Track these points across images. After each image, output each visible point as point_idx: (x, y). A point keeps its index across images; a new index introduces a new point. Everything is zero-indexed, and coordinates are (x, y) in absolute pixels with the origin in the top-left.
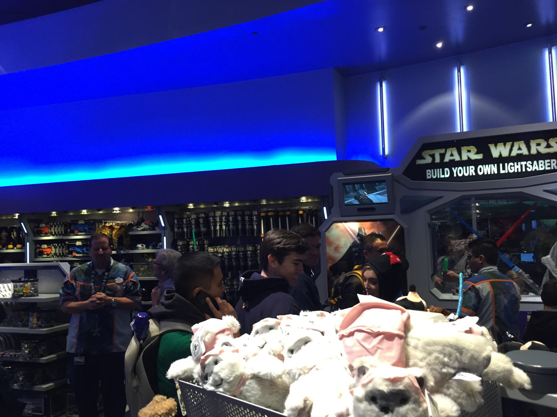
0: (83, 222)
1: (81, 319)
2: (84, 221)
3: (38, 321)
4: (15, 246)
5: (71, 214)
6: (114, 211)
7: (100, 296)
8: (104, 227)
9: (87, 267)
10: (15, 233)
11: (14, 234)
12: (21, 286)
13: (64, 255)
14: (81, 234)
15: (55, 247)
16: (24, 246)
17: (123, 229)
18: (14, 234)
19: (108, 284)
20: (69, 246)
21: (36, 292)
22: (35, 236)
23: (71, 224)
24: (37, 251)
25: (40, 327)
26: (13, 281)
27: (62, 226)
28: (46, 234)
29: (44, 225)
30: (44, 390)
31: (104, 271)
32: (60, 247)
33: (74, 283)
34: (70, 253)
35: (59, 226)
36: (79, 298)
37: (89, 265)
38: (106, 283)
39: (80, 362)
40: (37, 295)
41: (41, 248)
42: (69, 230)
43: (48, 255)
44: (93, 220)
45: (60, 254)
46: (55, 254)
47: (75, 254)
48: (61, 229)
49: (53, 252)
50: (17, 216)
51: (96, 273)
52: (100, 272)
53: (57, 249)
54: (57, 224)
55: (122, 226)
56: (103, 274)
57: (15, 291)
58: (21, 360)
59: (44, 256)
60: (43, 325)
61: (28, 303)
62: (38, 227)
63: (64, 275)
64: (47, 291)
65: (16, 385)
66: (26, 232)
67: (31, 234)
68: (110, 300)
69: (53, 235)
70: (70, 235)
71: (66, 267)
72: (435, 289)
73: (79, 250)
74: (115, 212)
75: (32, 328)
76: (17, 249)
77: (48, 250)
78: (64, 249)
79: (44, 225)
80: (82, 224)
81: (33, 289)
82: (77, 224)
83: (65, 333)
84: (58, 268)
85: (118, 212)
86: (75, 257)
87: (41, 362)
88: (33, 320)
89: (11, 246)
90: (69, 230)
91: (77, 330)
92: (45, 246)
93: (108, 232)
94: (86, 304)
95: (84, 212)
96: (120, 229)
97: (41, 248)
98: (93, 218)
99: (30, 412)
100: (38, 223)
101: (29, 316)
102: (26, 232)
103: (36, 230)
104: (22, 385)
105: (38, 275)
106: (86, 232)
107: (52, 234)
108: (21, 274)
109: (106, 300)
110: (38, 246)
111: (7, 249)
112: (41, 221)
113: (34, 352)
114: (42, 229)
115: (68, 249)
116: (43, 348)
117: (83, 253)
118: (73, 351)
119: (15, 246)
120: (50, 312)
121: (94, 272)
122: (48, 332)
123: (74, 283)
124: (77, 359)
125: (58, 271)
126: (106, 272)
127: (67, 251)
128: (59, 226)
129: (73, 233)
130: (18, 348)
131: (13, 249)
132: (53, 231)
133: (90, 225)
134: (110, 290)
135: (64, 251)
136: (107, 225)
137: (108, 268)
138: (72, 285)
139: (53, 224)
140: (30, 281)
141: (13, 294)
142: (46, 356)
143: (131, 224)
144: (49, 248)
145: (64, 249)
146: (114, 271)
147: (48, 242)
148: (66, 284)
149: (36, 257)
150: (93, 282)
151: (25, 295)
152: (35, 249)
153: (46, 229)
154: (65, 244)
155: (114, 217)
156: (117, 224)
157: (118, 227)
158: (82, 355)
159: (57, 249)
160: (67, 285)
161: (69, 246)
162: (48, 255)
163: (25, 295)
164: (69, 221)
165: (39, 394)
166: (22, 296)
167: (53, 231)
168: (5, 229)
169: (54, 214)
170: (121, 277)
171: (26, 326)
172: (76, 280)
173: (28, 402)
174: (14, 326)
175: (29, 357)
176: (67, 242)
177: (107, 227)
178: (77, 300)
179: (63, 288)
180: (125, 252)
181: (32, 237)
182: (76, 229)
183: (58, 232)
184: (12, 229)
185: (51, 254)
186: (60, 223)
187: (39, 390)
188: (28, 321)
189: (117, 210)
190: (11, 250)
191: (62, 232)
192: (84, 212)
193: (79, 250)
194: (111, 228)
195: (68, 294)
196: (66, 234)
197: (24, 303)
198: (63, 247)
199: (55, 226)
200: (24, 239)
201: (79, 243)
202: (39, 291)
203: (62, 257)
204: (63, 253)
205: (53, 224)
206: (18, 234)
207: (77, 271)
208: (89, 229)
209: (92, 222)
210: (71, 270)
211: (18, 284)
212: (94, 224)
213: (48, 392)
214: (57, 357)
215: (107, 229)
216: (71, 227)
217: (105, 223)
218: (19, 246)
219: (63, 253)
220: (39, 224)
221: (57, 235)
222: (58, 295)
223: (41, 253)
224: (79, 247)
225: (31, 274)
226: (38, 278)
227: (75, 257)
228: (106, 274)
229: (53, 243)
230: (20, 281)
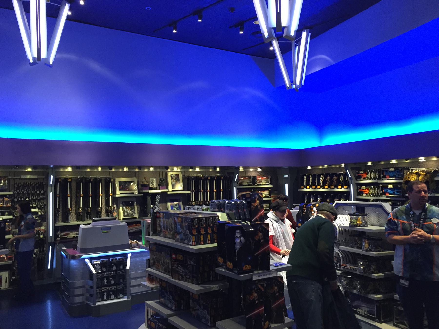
0: (393, 169)
1: (405, 250)
2: (394, 168)
3: (369, 246)
4: (342, 187)
5: (383, 163)
6: (419, 160)
7: (420, 233)
8: (412, 173)
9: (405, 208)
10: (342, 177)
11: (342, 179)
12: (355, 219)
13: (378, 195)
14: (391, 178)
15: (372, 189)
16: (349, 187)
17: (428, 175)
18: (342, 179)
19: (426, 223)
20: (382, 188)
21: (366, 224)
22: (356, 180)
23: (383, 171)
24: (359, 191)
25: (371, 250)
26: (350, 215)
27: (376, 172)
28: (364, 179)
29: (362, 172)
30: (376, 299)
31: (421, 212)
32: (375, 189)
33: (396, 221)
34: (384, 193)
35: (374, 172)
36: (402, 232)
37: (407, 207)
38: (424, 221)
39: (405, 284)
40: (367, 227)
41: (361, 189)
42: (382, 176)
43: (366, 194)
44: (401, 167)
45: (375, 194)
46: (372, 194)
47: (387, 195)
48: (376, 175)
49: (370, 192)
50: (343, 165)
51: (414, 214)
52: (417, 212)
53: (374, 190)
54: (372, 171)
55: (427, 173)
56: (421, 214)
57: (351, 222)
58: (357, 272)
59: (364, 195)
60: (373, 250)
61: (359, 231)
62: (359, 173)
63: (388, 214)
64: (374, 225)
65: (355, 290)
66: (350, 177)
67: (354, 178)
68: (430, 237)
69: (370, 180)
70: (383, 180)
71: (387, 206)
72: (31, 54)
73: (391, 192)
74: (420, 161)
75: (364, 250)
76: (344, 189)
77: (367, 190)
78: (379, 190)
79: (362, 172)
80: (392, 171)
81: (364, 221)
82: (389, 170)
83: (391, 258)
84: (381, 206)
85: (423, 160)
86: (387, 197)
87: (372, 277)
88: (365, 244)
89: (340, 187)
90: (382, 176)
91: (402, 259)
92: (364, 188)
93: (415, 178)
94: (408, 238)
95: (394, 161)
96: (425, 175)
97: (361, 189)
98: (400, 166)
99: (366, 313)
100: (359, 169)
101: (361, 241)
102: (350, 177)
103: (357, 175)
104: (359, 291)
105: (366, 211)
106: (397, 178)
107: (368, 178)
108: (353, 210)
109: (425, 237)
110: (359, 187)
111: (338, 188)
112: (360, 169)
113: (367, 268)
114: (361, 175)
115: (382, 191)
116: (374, 267)
117: (394, 194)
118: (401, 275)
119: (342, 187)
120: (376, 240)
121: (412, 213)
122: (377, 256)
123: (396, 221)
124: (402, 281)
125: (380, 209)
126: (423, 212)
127: (381, 192)
128: (374, 172)
129: (385, 177)
130: (355, 263)
131: (341, 189)
132: (369, 176)
133: (399, 172)
134: (428, 228)
135: (379, 192)
136: (414, 171)
137: (425, 210)
138: (395, 222)
139: (370, 171)
140: (362, 216)
141: (350, 224)
142: (376, 274)
143: (435, 171)
144: (367, 189)
145: (379, 190)
146: (430, 212)
147: (366, 185)
148: (390, 221)
149: (358, 195)
150: (412, 220)
151: (359, 225)
152: (357, 190)
153: (365, 174)
154: (379, 187)
155: (419, 165)
156: (423, 171)
157: (424, 174)
158: (407, 279)
159: (374, 190)
160: (390, 221)
161: (382, 188)
162: (366, 194)
163: (359, 225)
164: (382, 169)
165: (371, 301)
166: (357, 226)
167: (369, 176)
168: (336, 174)
169: (370, 163)
170: (436, 218)
171: (361, 248)
172: (397, 218)
173: (364, 305)
174: (352, 247)
175: (364, 272)
176: (381, 185)
177: (414, 173)
178: (400, 234)
179: (387, 224)
180: (432, 195)
181: (354, 181)
182: (388, 174)
183: (374, 177)
184: (340, 175)
185: (369, 193)
186: (375, 170)
187: (371, 298)
188: (361, 244)
189: (422, 159)
190: (340, 189)
191: (376, 177)
192: (394, 161)
193: (391, 192)
194: (418, 174)
195: (393, 229)
196: (380, 178)
197: (357, 231)
198: (378, 189)
199: (371, 173)
200: (349, 182)
201: (390, 186)
202: (368, 223)
203: (377, 196)
204: (378, 194)
205: (370, 171)
206: (345, 178)
207: (398, 211)
208: (398, 175)
209: (401, 169)
210: (392, 210)
211: (353, 217)
212: (402, 171)
213: (378, 301)
214: (385, 275)
215: (414, 175)
216: (383, 173)
217: (412, 170)
218: (345, 187)
219: (378, 194)
220: (359, 171)
221: (373, 180)
222: (384, 228)
223: (361, 193)
224: (390, 189)
225: (360, 210)
226: (366, 213)
227: (387, 197)
228: (423, 214)
229: (370, 186)
230: (354, 214)
